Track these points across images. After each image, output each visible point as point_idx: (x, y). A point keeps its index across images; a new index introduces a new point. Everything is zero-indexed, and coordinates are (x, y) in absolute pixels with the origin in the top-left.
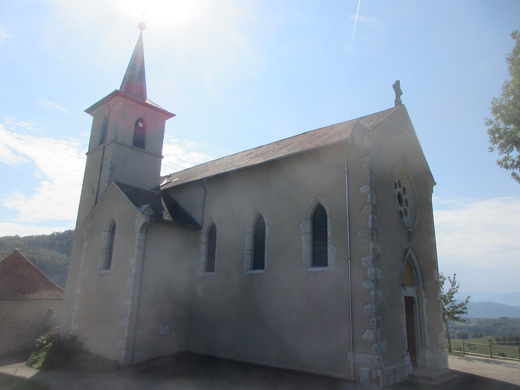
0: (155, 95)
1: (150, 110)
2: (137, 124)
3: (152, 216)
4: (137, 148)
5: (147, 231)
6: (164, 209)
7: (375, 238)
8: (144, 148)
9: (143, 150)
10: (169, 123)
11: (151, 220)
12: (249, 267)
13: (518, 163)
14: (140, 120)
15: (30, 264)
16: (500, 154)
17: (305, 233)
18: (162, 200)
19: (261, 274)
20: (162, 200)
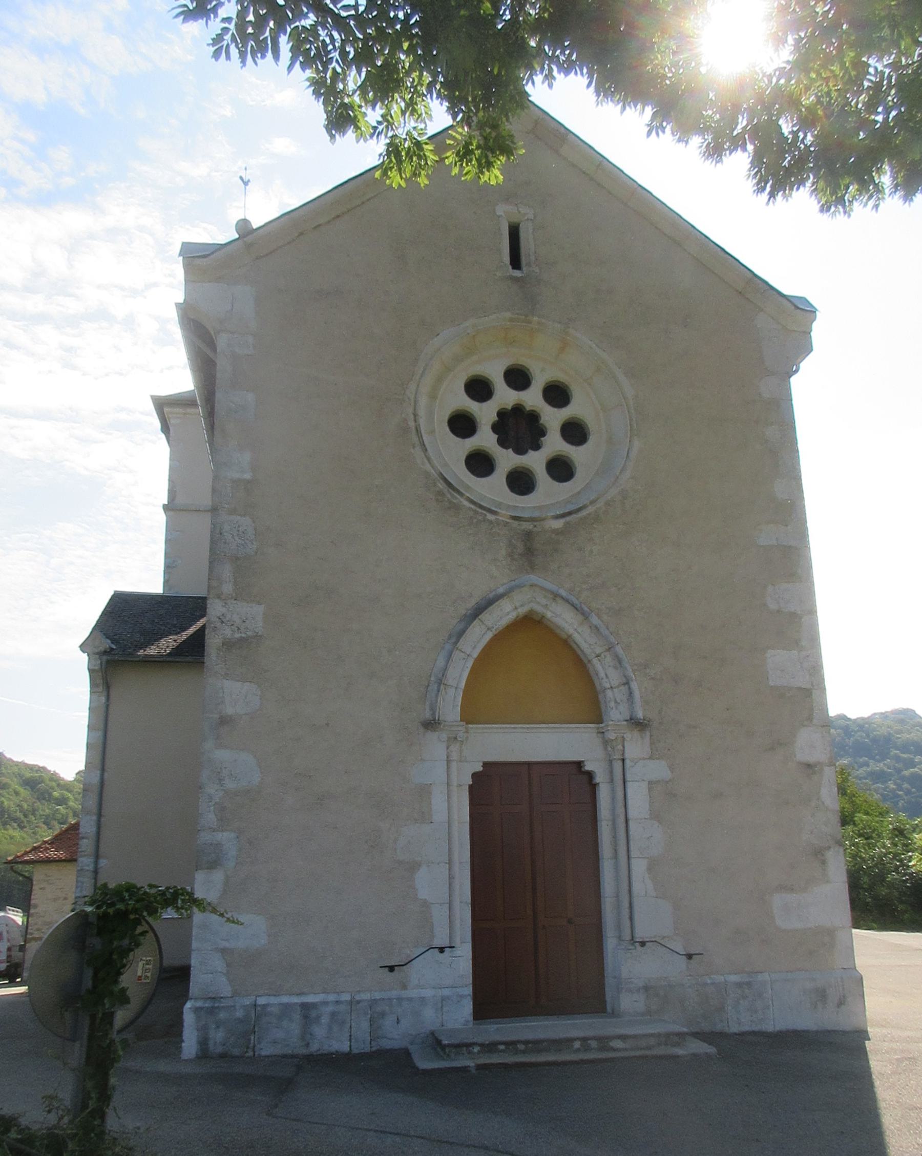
3: (105, 652)
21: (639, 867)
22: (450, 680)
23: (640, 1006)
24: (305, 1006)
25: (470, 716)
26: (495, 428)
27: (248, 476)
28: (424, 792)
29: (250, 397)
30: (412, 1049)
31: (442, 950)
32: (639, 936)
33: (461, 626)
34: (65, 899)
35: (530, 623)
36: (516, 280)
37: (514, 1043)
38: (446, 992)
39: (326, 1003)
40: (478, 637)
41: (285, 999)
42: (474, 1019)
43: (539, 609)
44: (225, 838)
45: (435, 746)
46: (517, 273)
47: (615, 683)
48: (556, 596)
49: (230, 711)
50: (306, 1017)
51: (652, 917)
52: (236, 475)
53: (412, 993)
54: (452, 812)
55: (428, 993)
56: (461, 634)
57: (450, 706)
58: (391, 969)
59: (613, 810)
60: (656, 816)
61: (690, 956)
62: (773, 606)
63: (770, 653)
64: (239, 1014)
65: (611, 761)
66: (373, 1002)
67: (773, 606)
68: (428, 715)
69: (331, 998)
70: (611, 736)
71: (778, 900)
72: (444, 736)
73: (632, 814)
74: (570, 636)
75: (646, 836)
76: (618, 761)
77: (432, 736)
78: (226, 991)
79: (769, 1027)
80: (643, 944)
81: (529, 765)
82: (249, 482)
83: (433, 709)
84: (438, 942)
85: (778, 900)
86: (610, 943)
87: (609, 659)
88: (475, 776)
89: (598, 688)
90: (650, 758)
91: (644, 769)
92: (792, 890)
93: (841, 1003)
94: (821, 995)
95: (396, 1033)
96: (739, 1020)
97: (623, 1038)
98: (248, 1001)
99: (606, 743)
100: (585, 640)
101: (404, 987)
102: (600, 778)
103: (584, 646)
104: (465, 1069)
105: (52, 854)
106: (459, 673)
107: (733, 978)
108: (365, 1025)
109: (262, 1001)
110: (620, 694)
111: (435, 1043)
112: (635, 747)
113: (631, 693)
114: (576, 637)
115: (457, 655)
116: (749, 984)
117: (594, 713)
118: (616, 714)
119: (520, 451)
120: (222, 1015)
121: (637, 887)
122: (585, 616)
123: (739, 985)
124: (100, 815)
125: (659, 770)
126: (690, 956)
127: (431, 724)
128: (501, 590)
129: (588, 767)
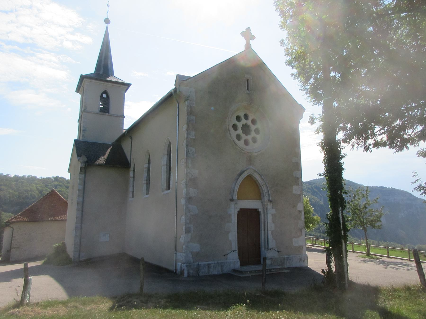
0: (119, 73)
1: (111, 84)
2: (102, 96)
3: (86, 162)
4: (103, 113)
5: (85, 172)
6: (104, 154)
7: (190, 165)
8: (108, 113)
9: (107, 114)
10: (128, 95)
11: (85, 165)
12: (145, 193)
13: (423, 289)
14: (105, 92)
15: (61, 198)
16: (285, 55)
17: (163, 165)
18: (110, 149)
19: (168, 193)
20: (110, 149)
21: (270, 232)
22: (235, 190)
23: (270, 263)
24: (208, 264)
25: (238, 199)
26: (242, 128)
27: (194, 138)
28: (230, 215)
29: (194, 117)
30: (230, 273)
31: (234, 251)
32: (270, 247)
33: (238, 177)
34: (26, 234)
35: (250, 177)
36: (248, 94)
37: (252, 271)
38: (235, 260)
39: (212, 263)
40: (241, 179)
41: (204, 263)
42: (240, 265)
43: (252, 174)
44: (191, 226)
45: (232, 205)
46: (248, 92)
47: (266, 192)
48: (255, 171)
49: (191, 195)
50: (208, 267)
51: (272, 244)
52: (192, 137)
53: (228, 261)
54: (234, 219)
55: (231, 261)
56: (237, 179)
57: (235, 197)
58: (224, 255)
59: (264, 220)
60: (273, 221)
61: (278, 252)
62: (294, 176)
63: (294, 186)
64: (195, 266)
65: (264, 209)
66: (221, 263)
67: (294, 176)
68: (231, 198)
69: (213, 262)
70: (265, 203)
71: (294, 240)
72: (234, 203)
73: (269, 221)
74: (257, 180)
75: (271, 226)
76: (265, 208)
77: (232, 202)
78: (192, 261)
79: (292, 266)
80: (270, 249)
81: (247, 209)
82: (194, 139)
83: (233, 197)
84: (233, 250)
85: (294, 240)
86: (263, 249)
87: (265, 186)
88: (238, 212)
89: (261, 191)
90: (272, 209)
91: (271, 211)
92: (296, 238)
93: (304, 261)
94: (301, 260)
95: (226, 270)
96: (287, 265)
97: (274, 269)
98: (197, 263)
99: (263, 205)
100: (260, 181)
101: (227, 259)
102: (262, 212)
103: (260, 183)
104: (249, 276)
105: (22, 219)
106: (237, 189)
107: (286, 256)
108: (220, 268)
109: (200, 263)
110: (266, 194)
111: (234, 270)
112: (270, 206)
113: (269, 194)
114: (259, 181)
115: (237, 184)
116: (289, 258)
117: (259, 196)
118: (266, 199)
119: (246, 135)
120: (192, 267)
121: (269, 237)
122: (261, 176)
123: (287, 258)
124: (82, 211)
125: (274, 211)
126: (278, 252)
127: (232, 200)
128: (245, 169)
129: (260, 210)
